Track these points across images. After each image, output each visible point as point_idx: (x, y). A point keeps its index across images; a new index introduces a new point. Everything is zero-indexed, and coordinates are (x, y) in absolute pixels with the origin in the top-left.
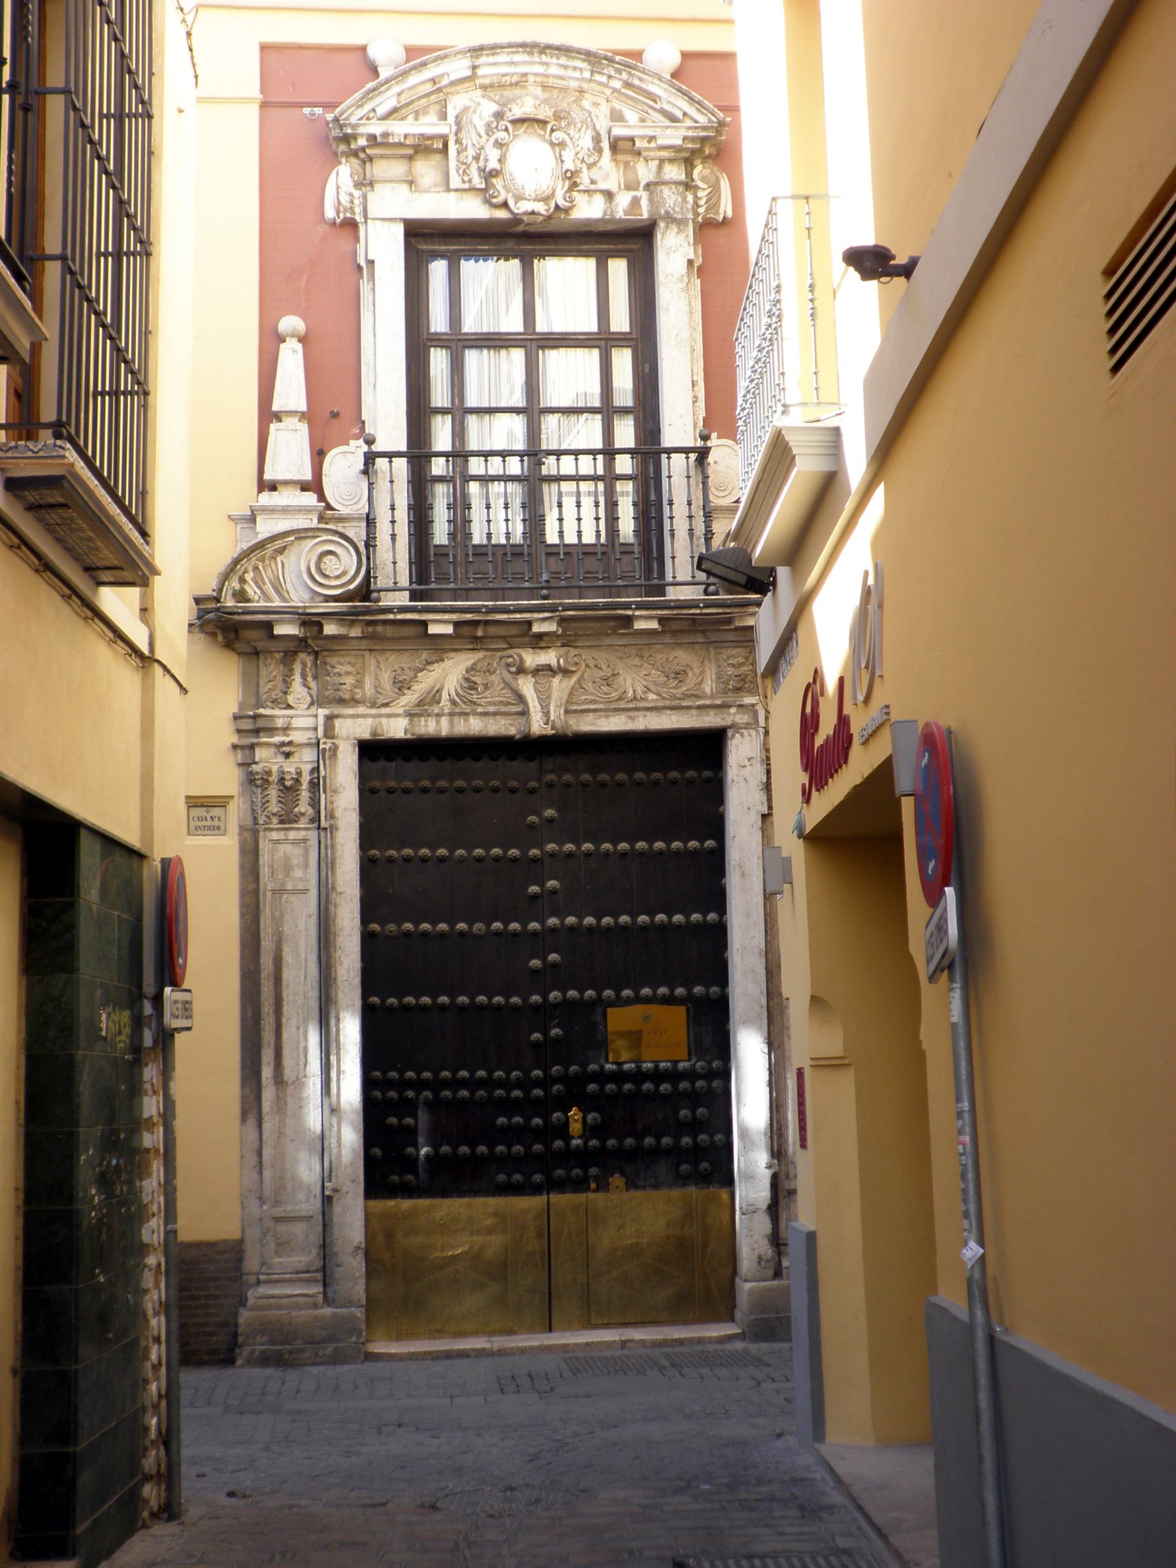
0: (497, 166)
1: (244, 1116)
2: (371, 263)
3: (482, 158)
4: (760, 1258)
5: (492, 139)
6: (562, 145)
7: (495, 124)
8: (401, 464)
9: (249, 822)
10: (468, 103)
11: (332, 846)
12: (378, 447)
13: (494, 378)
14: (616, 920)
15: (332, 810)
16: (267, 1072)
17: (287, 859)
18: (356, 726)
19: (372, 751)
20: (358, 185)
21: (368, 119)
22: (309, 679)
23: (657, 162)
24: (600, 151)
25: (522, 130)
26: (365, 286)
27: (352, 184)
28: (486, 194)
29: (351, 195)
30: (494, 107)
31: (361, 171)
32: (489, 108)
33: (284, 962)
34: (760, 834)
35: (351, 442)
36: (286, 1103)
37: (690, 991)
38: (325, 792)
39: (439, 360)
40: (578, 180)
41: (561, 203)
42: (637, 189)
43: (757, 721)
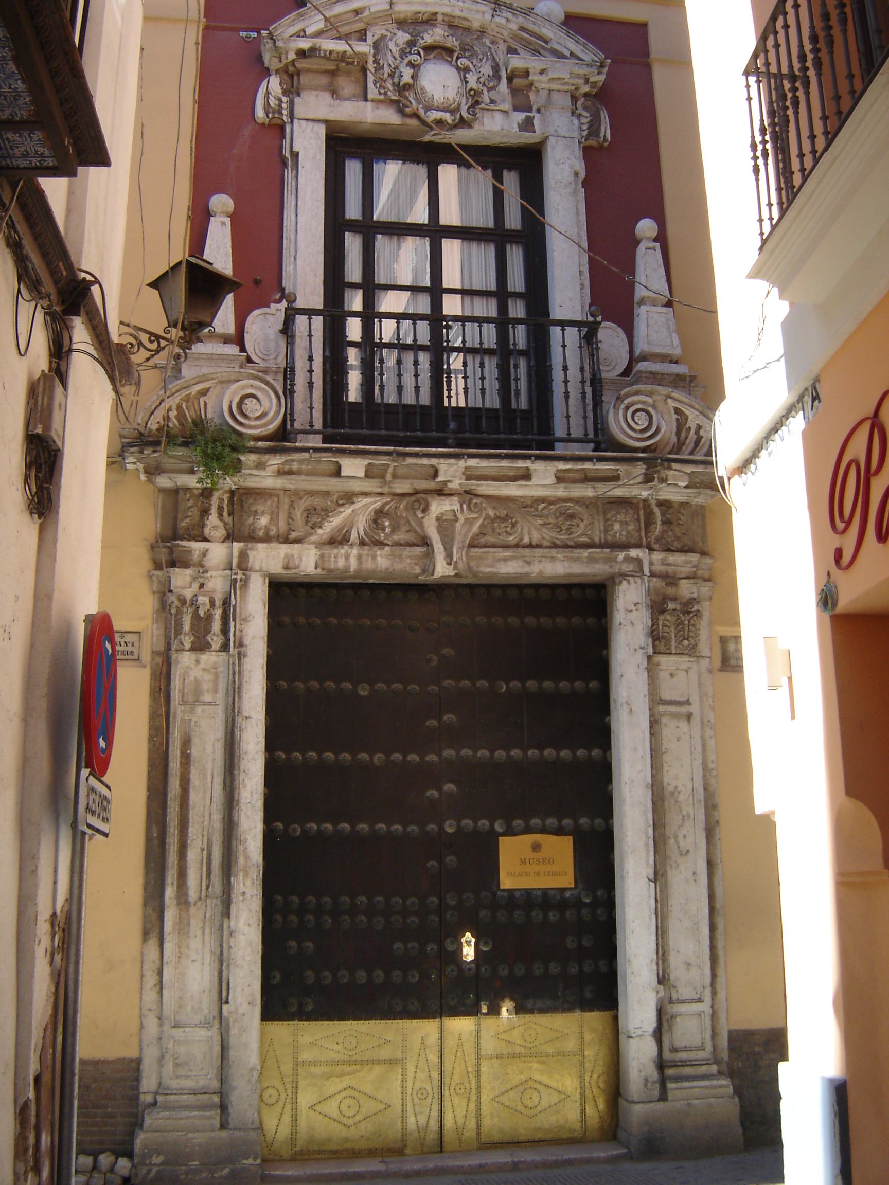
0: (411, 81)
1: (146, 934)
2: (295, 156)
3: (396, 75)
4: (646, 1080)
5: (406, 61)
6: (467, 70)
7: (408, 50)
8: (318, 321)
9: (161, 647)
10: (385, 33)
11: (239, 672)
12: (300, 304)
13: (405, 261)
14: (405, 757)
15: (241, 638)
16: (170, 892)
17: (197, 683)
18: (269, 559)
19: (282, 591)
20: (285, 93)
21: (299, 36)
22: (225, 514)
23: (547, 92)
24: (499, 78)
25: (432, 56)
26: (289, 174)
27: (280, 91)
28: (400, 107)
29: (280, 101)
30: (407, 37)
31: (289, 81)
32: (403, 37)
33: (191, 784)
34: (646, 674)
35: (272, 305)
36: (189, 924)
37: (576, 822)
38: (234, 620)
39: (353, 244)
40: (480, 100)
41: (465, 115)
42: (531, 111)
43: (642, 571)
